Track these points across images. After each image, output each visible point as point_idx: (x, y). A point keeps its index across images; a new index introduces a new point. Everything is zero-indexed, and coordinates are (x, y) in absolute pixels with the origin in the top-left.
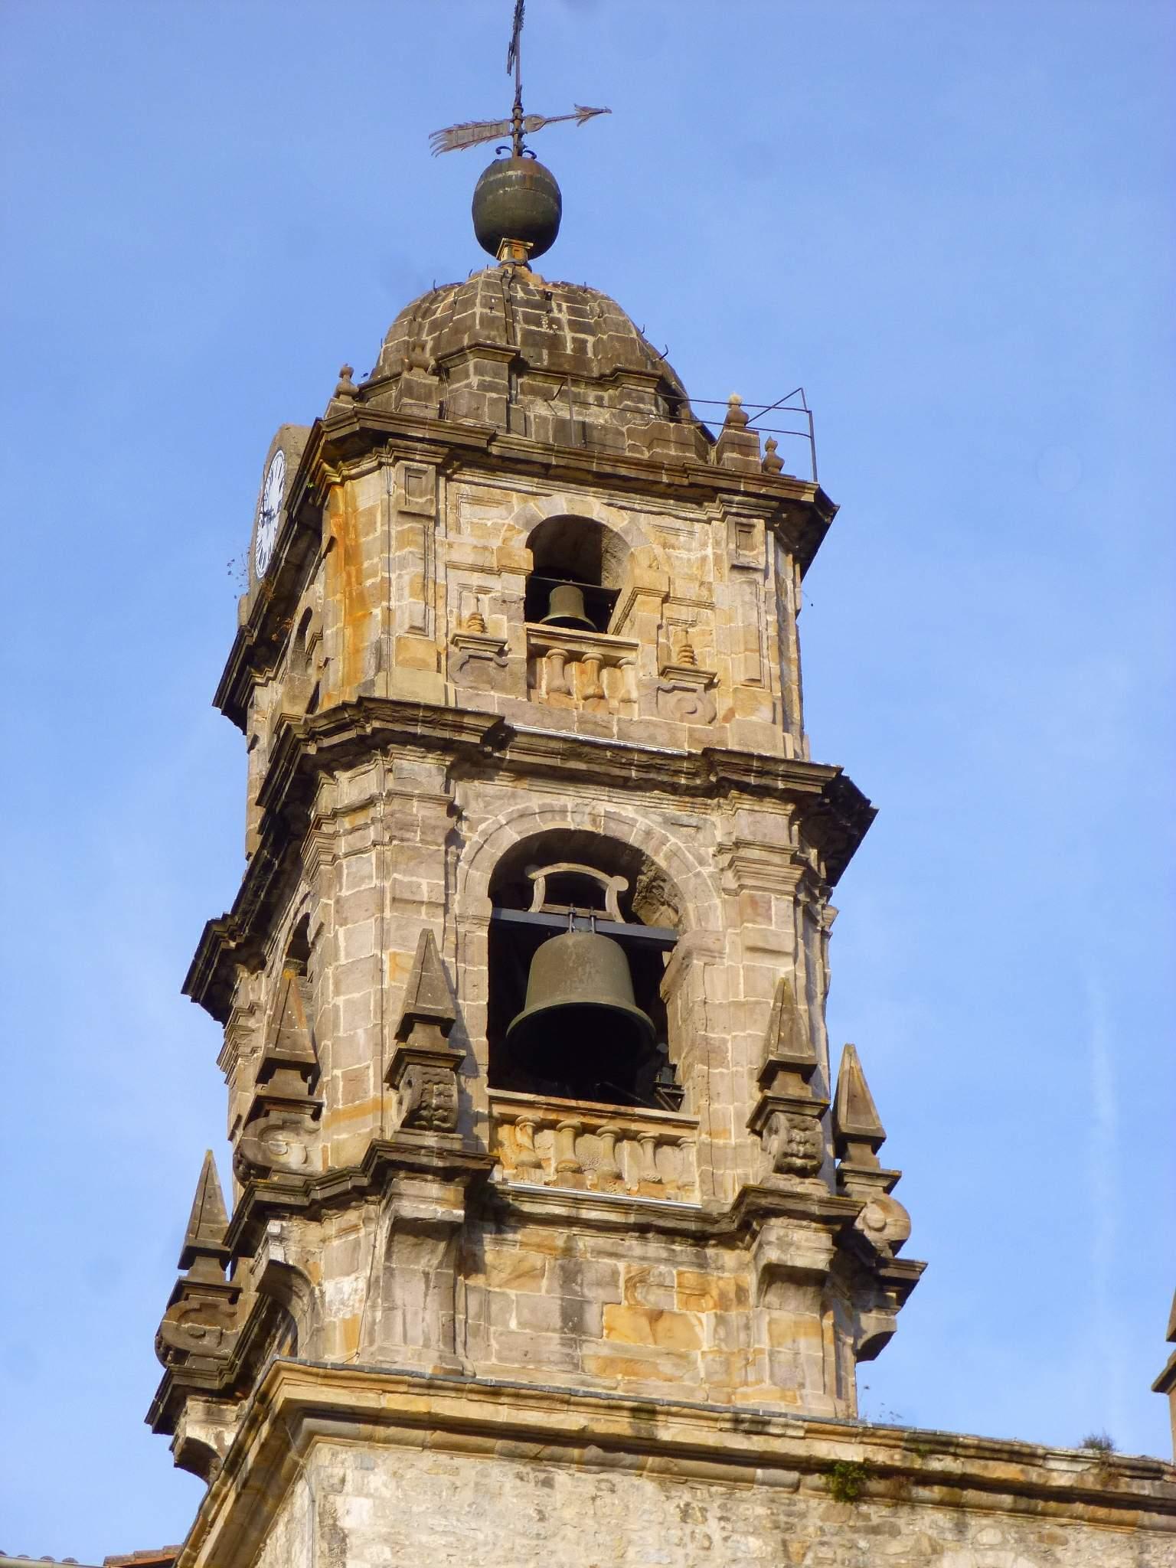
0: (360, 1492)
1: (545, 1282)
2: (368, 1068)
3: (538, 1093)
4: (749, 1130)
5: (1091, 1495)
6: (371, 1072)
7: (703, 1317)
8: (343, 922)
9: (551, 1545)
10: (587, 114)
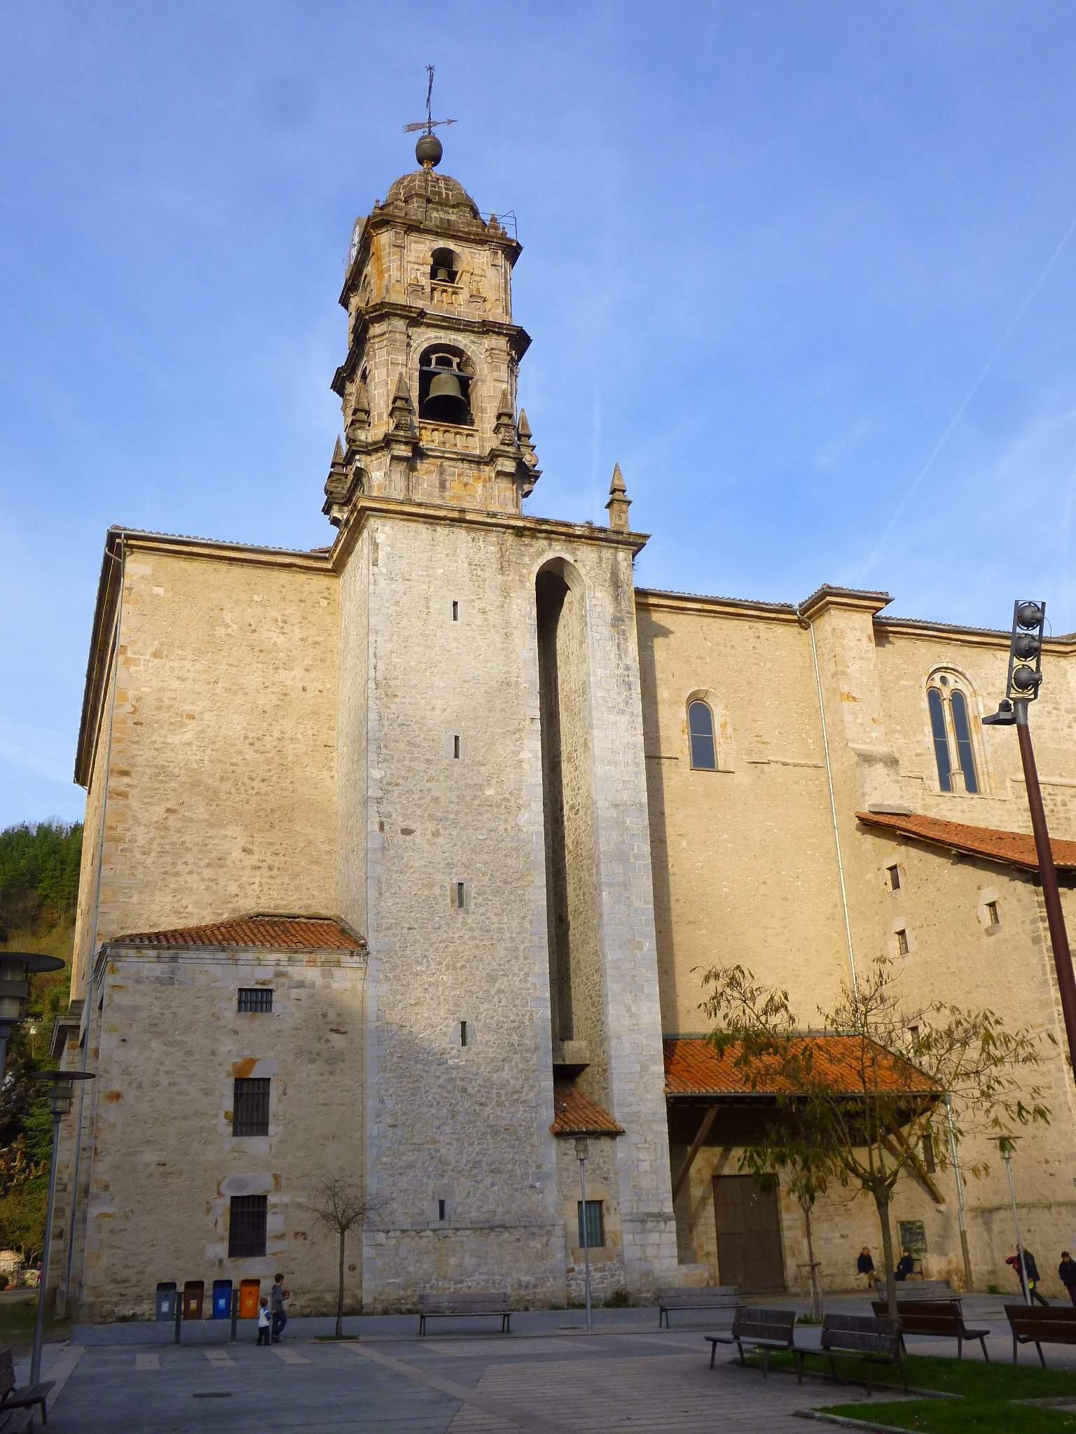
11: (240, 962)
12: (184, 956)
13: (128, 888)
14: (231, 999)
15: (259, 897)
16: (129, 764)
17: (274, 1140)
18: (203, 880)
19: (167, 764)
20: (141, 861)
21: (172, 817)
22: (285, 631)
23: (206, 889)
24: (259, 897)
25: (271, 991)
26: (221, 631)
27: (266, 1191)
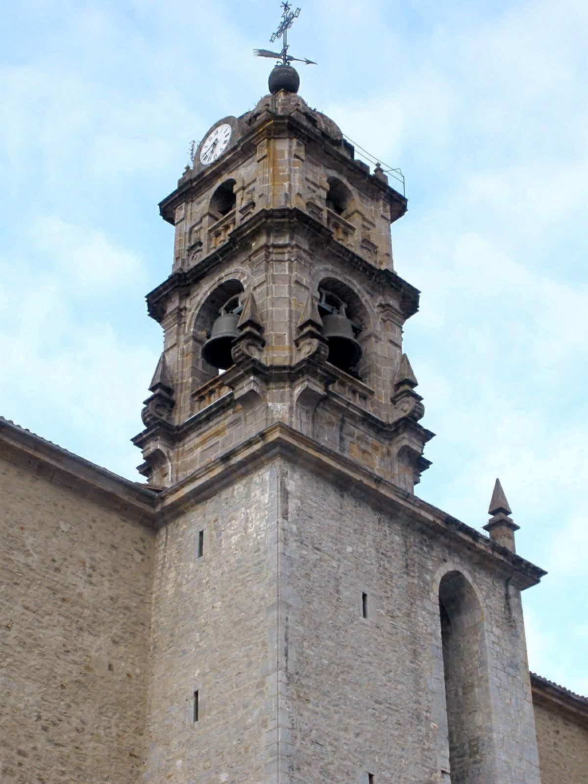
0: (292, 478)
1: (334, 428)
2: (285, 334)
3: (332, 364)
4: (146, 299)
5: (292, 438)
6: (286, 336)
7: (377, 457)
8: (274, 283)
9: (344, 518)
10: (308, 62)
22: (93, 580)
26: (18, 557)
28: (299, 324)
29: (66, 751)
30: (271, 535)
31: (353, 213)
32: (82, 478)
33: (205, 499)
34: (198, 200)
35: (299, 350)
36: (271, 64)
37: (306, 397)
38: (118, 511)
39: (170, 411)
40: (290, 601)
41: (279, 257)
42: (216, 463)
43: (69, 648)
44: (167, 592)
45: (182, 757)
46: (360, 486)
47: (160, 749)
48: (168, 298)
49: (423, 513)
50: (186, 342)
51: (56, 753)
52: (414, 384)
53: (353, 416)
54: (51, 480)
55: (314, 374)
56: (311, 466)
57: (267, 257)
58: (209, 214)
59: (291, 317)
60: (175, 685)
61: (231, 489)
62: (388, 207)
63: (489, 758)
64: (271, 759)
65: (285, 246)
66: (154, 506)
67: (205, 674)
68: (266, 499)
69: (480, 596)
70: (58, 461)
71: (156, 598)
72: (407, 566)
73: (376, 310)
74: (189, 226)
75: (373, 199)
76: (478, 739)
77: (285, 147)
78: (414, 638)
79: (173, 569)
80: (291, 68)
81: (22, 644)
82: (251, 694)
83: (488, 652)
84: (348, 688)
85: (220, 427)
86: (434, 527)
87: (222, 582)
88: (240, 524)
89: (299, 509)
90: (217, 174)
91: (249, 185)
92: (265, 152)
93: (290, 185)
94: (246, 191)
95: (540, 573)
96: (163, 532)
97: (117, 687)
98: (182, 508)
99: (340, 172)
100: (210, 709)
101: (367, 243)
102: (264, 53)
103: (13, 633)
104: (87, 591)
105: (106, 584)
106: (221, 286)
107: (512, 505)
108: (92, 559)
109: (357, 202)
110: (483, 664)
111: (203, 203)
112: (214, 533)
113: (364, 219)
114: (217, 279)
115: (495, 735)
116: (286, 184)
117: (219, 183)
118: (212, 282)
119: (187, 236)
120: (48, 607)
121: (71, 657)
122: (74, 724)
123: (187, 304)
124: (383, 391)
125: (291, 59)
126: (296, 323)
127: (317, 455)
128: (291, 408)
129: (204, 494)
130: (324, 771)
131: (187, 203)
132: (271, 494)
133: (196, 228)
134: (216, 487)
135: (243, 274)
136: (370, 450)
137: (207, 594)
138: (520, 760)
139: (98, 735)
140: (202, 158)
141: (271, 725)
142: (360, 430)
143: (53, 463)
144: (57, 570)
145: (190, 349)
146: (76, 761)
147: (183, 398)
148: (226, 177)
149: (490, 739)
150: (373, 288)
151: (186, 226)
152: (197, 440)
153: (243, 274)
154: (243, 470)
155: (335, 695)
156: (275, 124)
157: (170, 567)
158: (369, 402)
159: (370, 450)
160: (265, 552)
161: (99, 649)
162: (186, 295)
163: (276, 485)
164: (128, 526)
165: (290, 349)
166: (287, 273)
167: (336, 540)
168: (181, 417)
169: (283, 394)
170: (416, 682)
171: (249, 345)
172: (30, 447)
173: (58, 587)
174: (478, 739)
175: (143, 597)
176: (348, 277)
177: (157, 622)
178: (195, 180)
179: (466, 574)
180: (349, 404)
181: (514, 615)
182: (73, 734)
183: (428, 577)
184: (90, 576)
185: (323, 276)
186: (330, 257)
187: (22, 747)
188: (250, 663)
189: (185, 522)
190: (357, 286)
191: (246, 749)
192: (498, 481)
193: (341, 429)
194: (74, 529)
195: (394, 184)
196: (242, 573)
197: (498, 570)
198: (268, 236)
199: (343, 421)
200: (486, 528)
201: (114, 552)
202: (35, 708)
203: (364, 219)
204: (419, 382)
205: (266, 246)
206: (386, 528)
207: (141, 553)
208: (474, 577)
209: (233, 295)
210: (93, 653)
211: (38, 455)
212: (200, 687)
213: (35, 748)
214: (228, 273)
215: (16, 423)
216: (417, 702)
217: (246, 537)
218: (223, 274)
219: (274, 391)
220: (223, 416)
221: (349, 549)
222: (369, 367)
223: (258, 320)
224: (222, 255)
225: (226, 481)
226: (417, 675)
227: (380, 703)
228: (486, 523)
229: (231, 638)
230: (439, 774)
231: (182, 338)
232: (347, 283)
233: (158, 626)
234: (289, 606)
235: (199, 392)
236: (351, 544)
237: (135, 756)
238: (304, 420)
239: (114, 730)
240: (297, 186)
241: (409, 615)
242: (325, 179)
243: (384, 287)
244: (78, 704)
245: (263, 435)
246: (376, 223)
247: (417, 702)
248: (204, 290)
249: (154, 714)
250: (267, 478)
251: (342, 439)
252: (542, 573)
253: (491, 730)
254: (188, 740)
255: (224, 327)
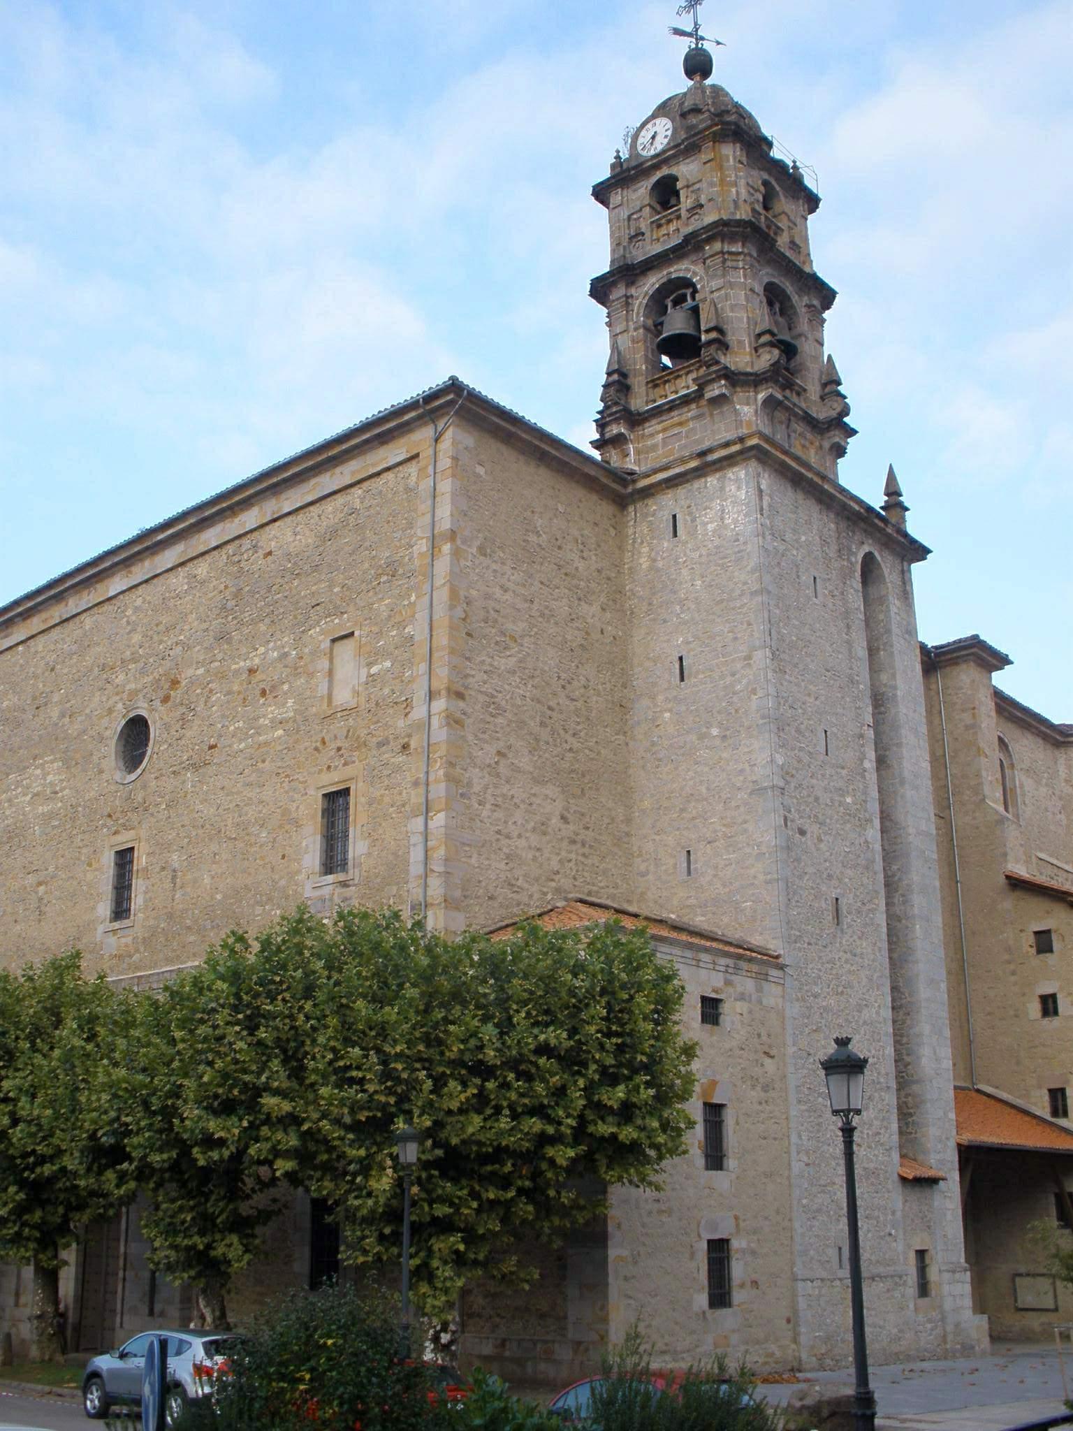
11: (701, 964)
12: (663, 949)
13: (468, 845)
14: (695, 1007)
15: (575, 879)
16: (463, 685)
17: (734, 1176)
18: (530, 847)
19: (495, 694)
20: (478, 812)
21: (503, 762)
22: (585, 555)
23: (533, 860)
24: (575, 879)
25: (720, 1000)
26: (533, 538)
27: (730, 1234)
28: (757, 331)
29: (579, 704)
30: (750, 528)
31: (780, 214)
32: (574, 464)
33: (676, 485)
34: (634, 187)
35: (759, 356)
36: (685, 45)
37: (770, 403)
38: (597, 492)
39: (626, 395)
40: (770, 588)
41: (734, 264)
42: (691, 458)
43: (574, 616)
44: (641, 565)
45: (670, 711)
46: (811, 483)
47: (645, 702)
48: (614, 284)
49: (852, 504)
50: (636, 329)
51: (572, 706)
52: (839, 383)
53: (796, 415)
54: (548, 466)
55: (776, 382)
56: (777, 466)
57: (724, 261)
58: (649, 205)
59: (748, 323)
60: (658, 649)
61: (703, 480)
62: (806, 206)
63: (893, 711)
64: (761, 722)
65: (739, 254)
66: (625, 487)
67: (688, 643)
68: (742, 495)
69: (886, 571)
70: (557, 449)
71: (630, 569)
72: (840, 551)
73: (804, 310)
74: (627, 214)
75: (793, 197)
76: (883, 694)
77: (731, 152)
78: (847, 614)
79: (645, 544)
80: (705, 50)
81: (542, 615)
82: (739, 666)
83: (893, 621)
84: (809, 660)
85: (684, 418)
86: (858, 514)
87: (700, 564)
88: (716, 514)
89: (770, 506)
90: (656, 167)
91: (694, 184)
92: (712, 156)
93: (737, 191)
94: (691, 189)
95: (928, 551)
96: (631, 509)
97: (608, 648)
98: (653, 491)
99: (770, 174)
100: (697, 672)
101: (794, 245)
102: (678, 32)
103: (535, 606)
104: (581, 565)
105: (594, 558)
106: (670, 281)
107: (903, 488)
108: (582, 536)
109: (784, 204)
110: (888, 631)
111: (642, 192)
112: (688, 518)
113: (789, 220)
114: (665, 273)
115: (899, 693)
116: (734, 190)
117: (658, 175)
118: (660, 275)
119: (626, 223)
120: (556, 581)
121: (576, 624)
122: (582, 682)
123: (633, 291)
124: (814, 390)
125: (702, 39)
126: (754, 331)
127: (783, 457)
128: (756, 411)
129: (676, 481)
130: (798, 731)
131: (623, 189)
132: (747, 492)
133: (635, 216)
134: (688, 477)
135: (695, 274)
136: (807, 444)
137: (685, 572)
138: (915, 711)
139: (598, 690)
140: (640, 148)
141: (760, 693)
142: (799, 427)
143: (554, 452)
144: (560, 548)
145: (641, 337)
146: (585, 713)
147: (638, 384)
148: (665, 171)
149: (895, 695)
150: (800, 289)
151: (624, 213)
152: (659, 427)
153: (695, 274)
154: (718, 466)
155: (801, 666)
156: (722, 129)
157: (642, 542)
158: (802, 398)
159: (807, 444)
160: (745, 543)
161: (593, 616)
162: (631, 283)
163: (753, 484)
164: (604, 503)
165: (751, 355)
166: (742, 280)
167: (794, 531)
168: (639, 403)
169: (748, 398)
170: (850, 651)
171: (717, 349)
172: (535, 437)
173: (562, 563)
174: (883, 694)
175: (618, 566)
176: (783, 279)
177: (631, 590)
178: (634, 168)
179: (876, 554)
180: (795, 405)
181: (908, 588)
182: (582, 690)
183: (853, 560)
184: (582, 551)
185: (766, 280)
186: (770, 262)
187: (551, 703)
188: (736, 639)
189: (656, 504)
190: (789, 287)
191: (737, 711)
192: (891, 468)
193: (788, 427)
194: (568, 510)
195: (809, 182)
196: (722, 558)
197: (898, 549)
198: (723, 242)
199: (790, 420)
200: (882, 508)
201: (597, 529)
202: (556, 670)
203: (789, 220)
204: (843, 381)
205: (722, 253)
206: (825, 518)
207: (615, 528)
208: (881, 556)
209: (680, 289)
210: (589, 620)
211: (543, 446)
212: (684, 654)
213: (558, 704)
214: (680, 269)
215: (484, 394)
216: (851, 668)
217: (723, 526)
218: (672, 270)
219: (740, 395)
220: (686, 409)
221: (803, 538)
222: (800, 364)
223: (721, 325)
224: (673, 253)
225: (699, 472)
226: (849, 643)
227: (828, 671)
228: (883, 504)
229: (714, 614)
230: (866, 728)
231: (632, 326)
232: (780, 284)
233: (634, 595)
234: (769, 592)
235: (653, 381)
236: (805, 534)
237: (623, 707)
238: (766, 422)
239: (608, 686)
240: (743, 191)
241: (842, 593)
242: (760, 182)
243: (809, 289)
244: (582, 664)
245: (741, 440)
246: (798, 223)
247: (851, 668)
248: (652, 282)
249: (636, 670)
250: (743, 476)
251: (789, 436)
252: (929, 551)
253: (895, 688)
254: (675, 697)
255: (676, 323)
